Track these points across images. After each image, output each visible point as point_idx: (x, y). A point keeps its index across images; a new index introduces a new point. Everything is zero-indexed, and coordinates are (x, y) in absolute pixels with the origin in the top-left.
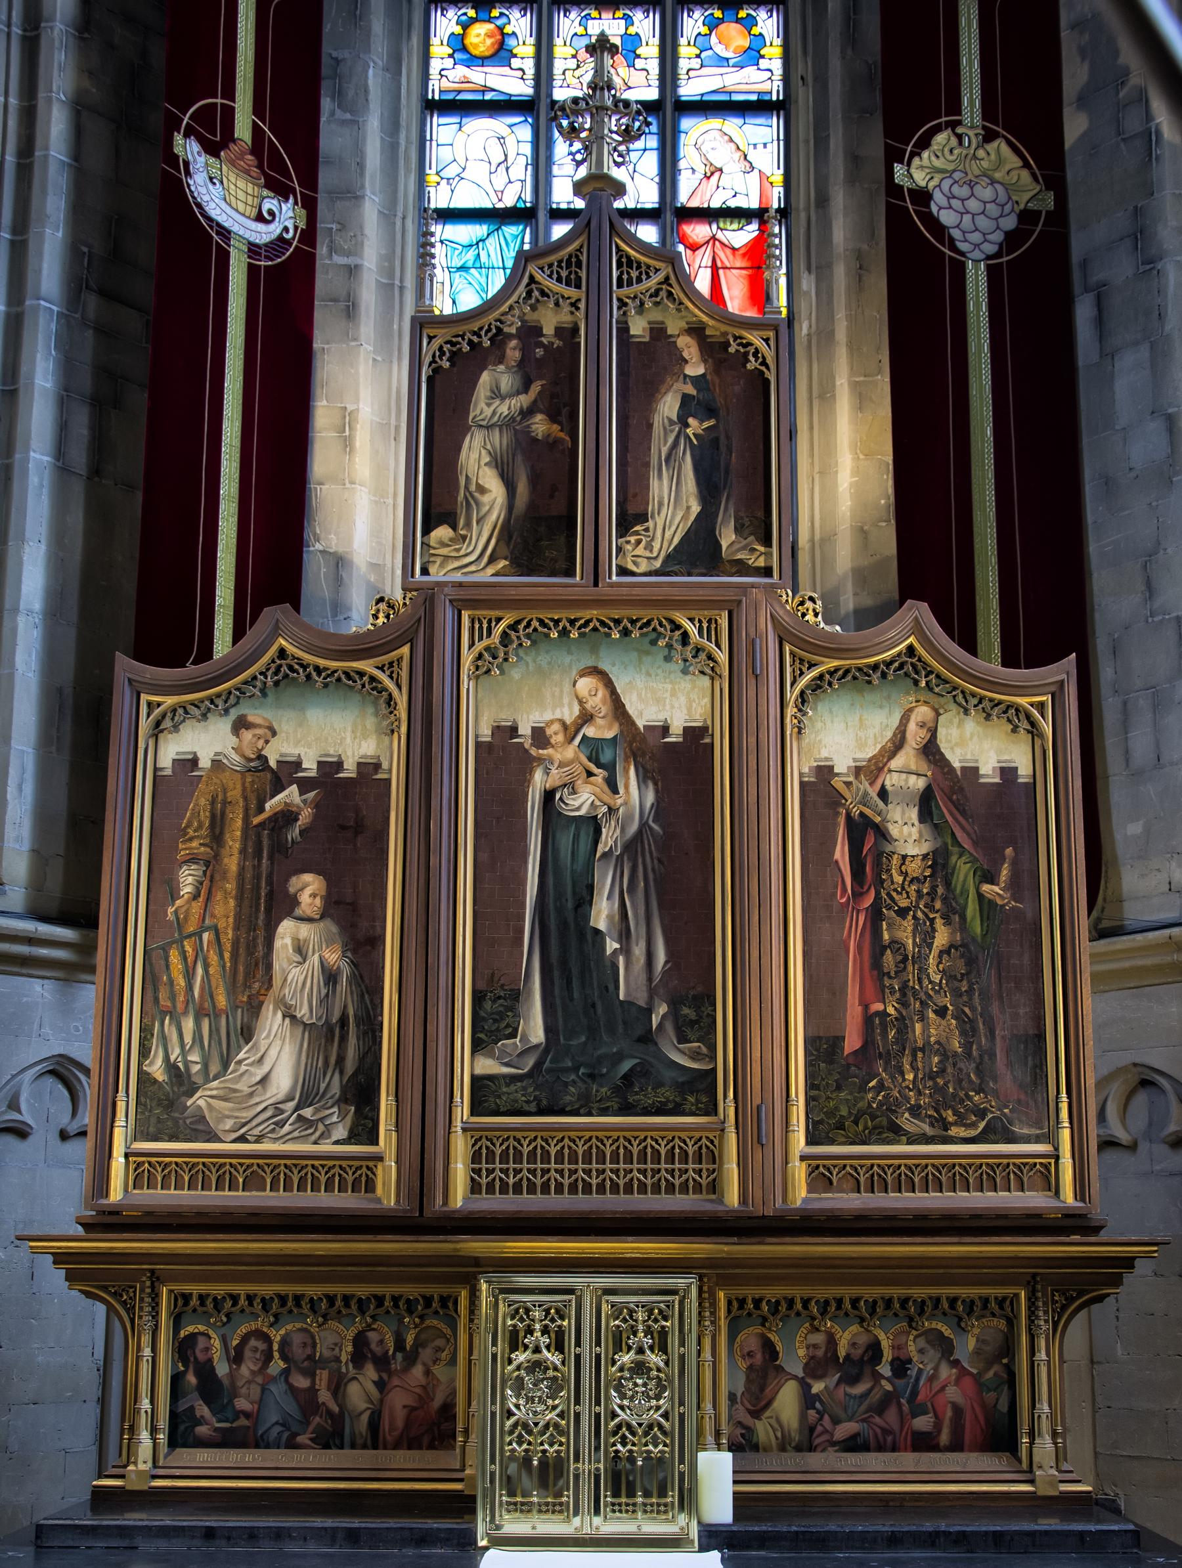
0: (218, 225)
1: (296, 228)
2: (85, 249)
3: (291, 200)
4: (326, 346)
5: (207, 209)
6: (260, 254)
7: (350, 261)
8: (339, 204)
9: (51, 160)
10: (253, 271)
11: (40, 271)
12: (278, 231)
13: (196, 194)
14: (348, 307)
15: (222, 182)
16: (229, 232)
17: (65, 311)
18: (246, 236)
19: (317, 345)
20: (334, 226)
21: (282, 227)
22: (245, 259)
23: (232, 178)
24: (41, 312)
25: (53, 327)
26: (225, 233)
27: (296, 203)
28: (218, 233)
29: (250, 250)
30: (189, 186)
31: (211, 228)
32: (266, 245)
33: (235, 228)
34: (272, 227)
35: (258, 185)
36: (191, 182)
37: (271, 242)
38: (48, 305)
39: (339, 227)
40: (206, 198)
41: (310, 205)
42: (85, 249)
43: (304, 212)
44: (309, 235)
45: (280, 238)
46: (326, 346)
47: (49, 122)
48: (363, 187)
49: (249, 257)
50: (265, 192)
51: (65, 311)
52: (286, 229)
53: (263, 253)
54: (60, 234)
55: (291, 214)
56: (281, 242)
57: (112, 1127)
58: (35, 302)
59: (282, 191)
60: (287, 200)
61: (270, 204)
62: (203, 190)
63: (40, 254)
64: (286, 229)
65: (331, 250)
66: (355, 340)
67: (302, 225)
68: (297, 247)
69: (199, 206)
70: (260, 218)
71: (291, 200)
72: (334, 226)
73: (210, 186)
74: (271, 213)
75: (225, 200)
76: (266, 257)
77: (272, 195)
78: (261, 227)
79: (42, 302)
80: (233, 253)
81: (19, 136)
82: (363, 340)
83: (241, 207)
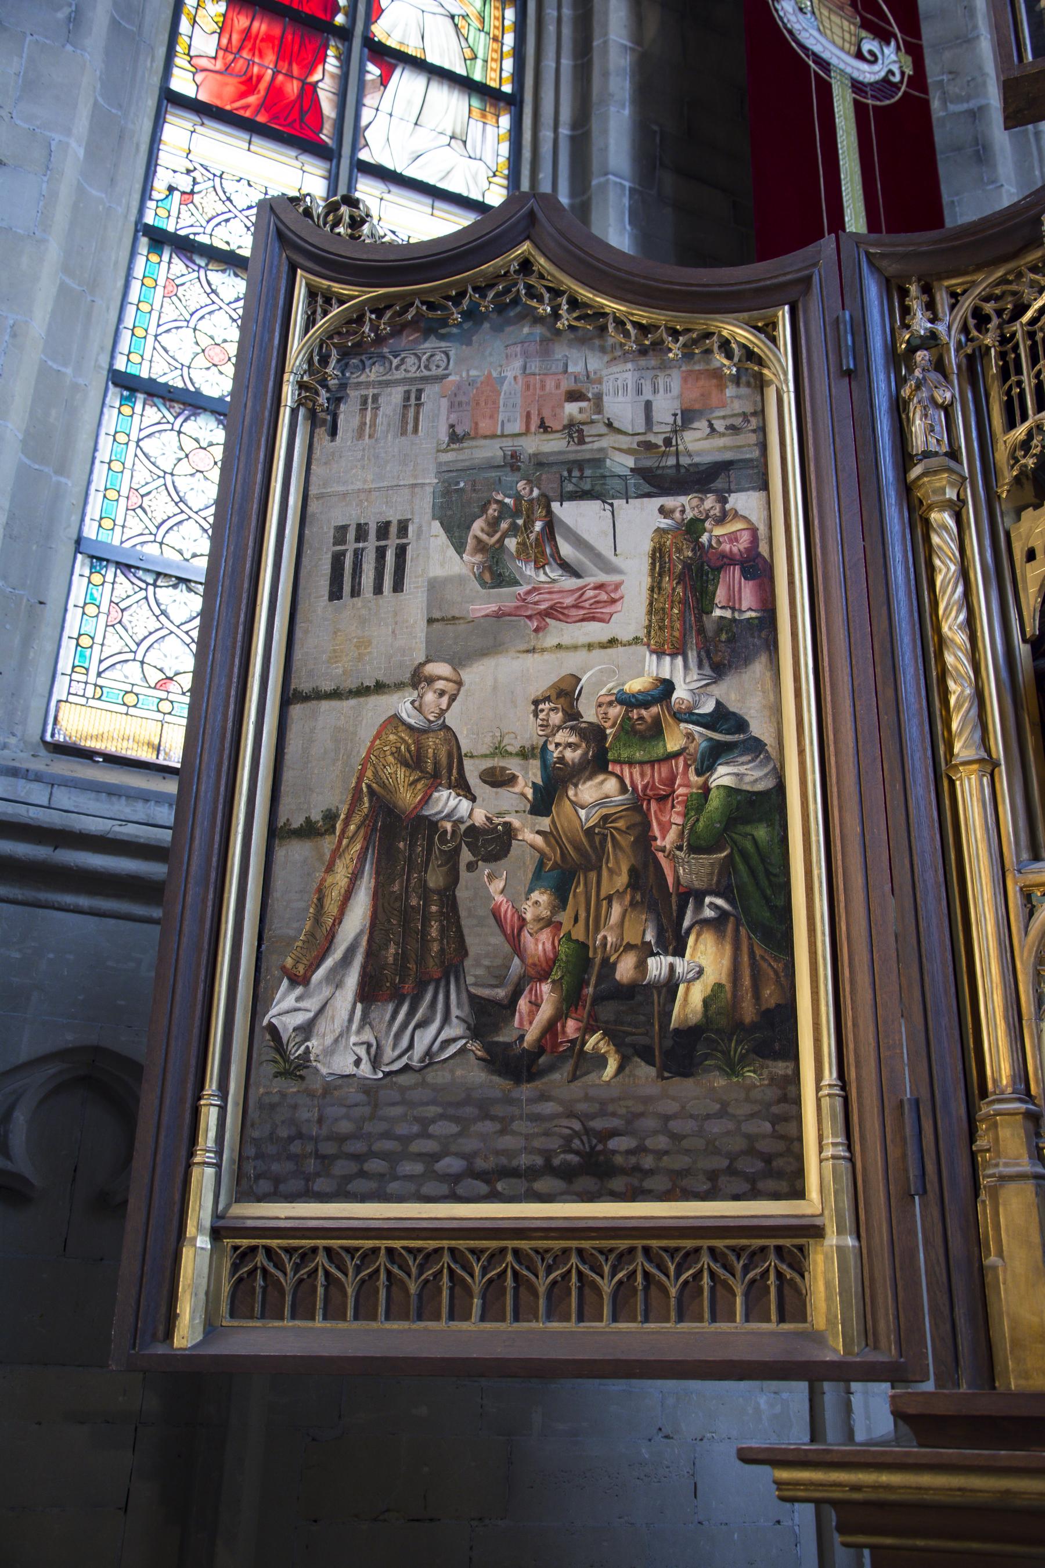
0: (814, 54)
1: (903, 74)
2: (656, 128)
3: (893, 43)
4: (956, 199)
5: (799, 37)
6: (866, 93)
7: (972, 104)
8: (947, 55)
9: (611, 44)
10: (860, 108)
11: (605, 149)
12: (883, 74)
13: (785, 20)
14: (978, 151)
15: (813, 13)
16: (829, 64)
17: (637, 187)
18: (849, 70)
19: (946, 198)
20: (945, 77)
21: (885, 70)
22: (849, 96)
23: (825, 12)
24: (611, 187)
25: (626, 201)
26: (825, 65)
27: (898, 48)
28: (814, 62)
29: (853, 86)
30: (777, 10)
31: (808, 57)
32: (871, 84)
33: (834, 61)
34: (876, 68)
35: (854, 24)
36: (779, 7)
37: (877, 82)
38: (618, 180)
39: (951, 77)
40: (797, 26)
41: (915, 51)
42: (656, 128)
43: (909, 59)
44: (918, 79)
45: (886, 80)
46: (956, 199)
47: (606, 13)
48: (975, 27)
49: (854, 92)
50: (864, 33)
51: (637, 187)
52: (891, 72)
53: (870, 93)
54: (626, 112)
55: (893, 57)
56: (886, 84)
57: (189, 1166)
58: (602, 179)
59: (884, 37)
60: (888, 44)
61: (869, 45)
62: (793, 19)
63: (605, 132)
64: (891, 72)
65: (944, 102)
66: (993, 182)
67: (909, 71)
68: (905, 92)
69: (790, 32)
70: (859, 56)
71: (893, 43)
72: (945, 77)
73: (800, 16)
74: (871, 52)
75: (819, 30)
76: (872, 96)
77: (872, 37)
78: (865, 67)
79: (611, 177)
80: (836, 90)
81: (575, 42)
82: (1002, 180)
83: (839, 41)
